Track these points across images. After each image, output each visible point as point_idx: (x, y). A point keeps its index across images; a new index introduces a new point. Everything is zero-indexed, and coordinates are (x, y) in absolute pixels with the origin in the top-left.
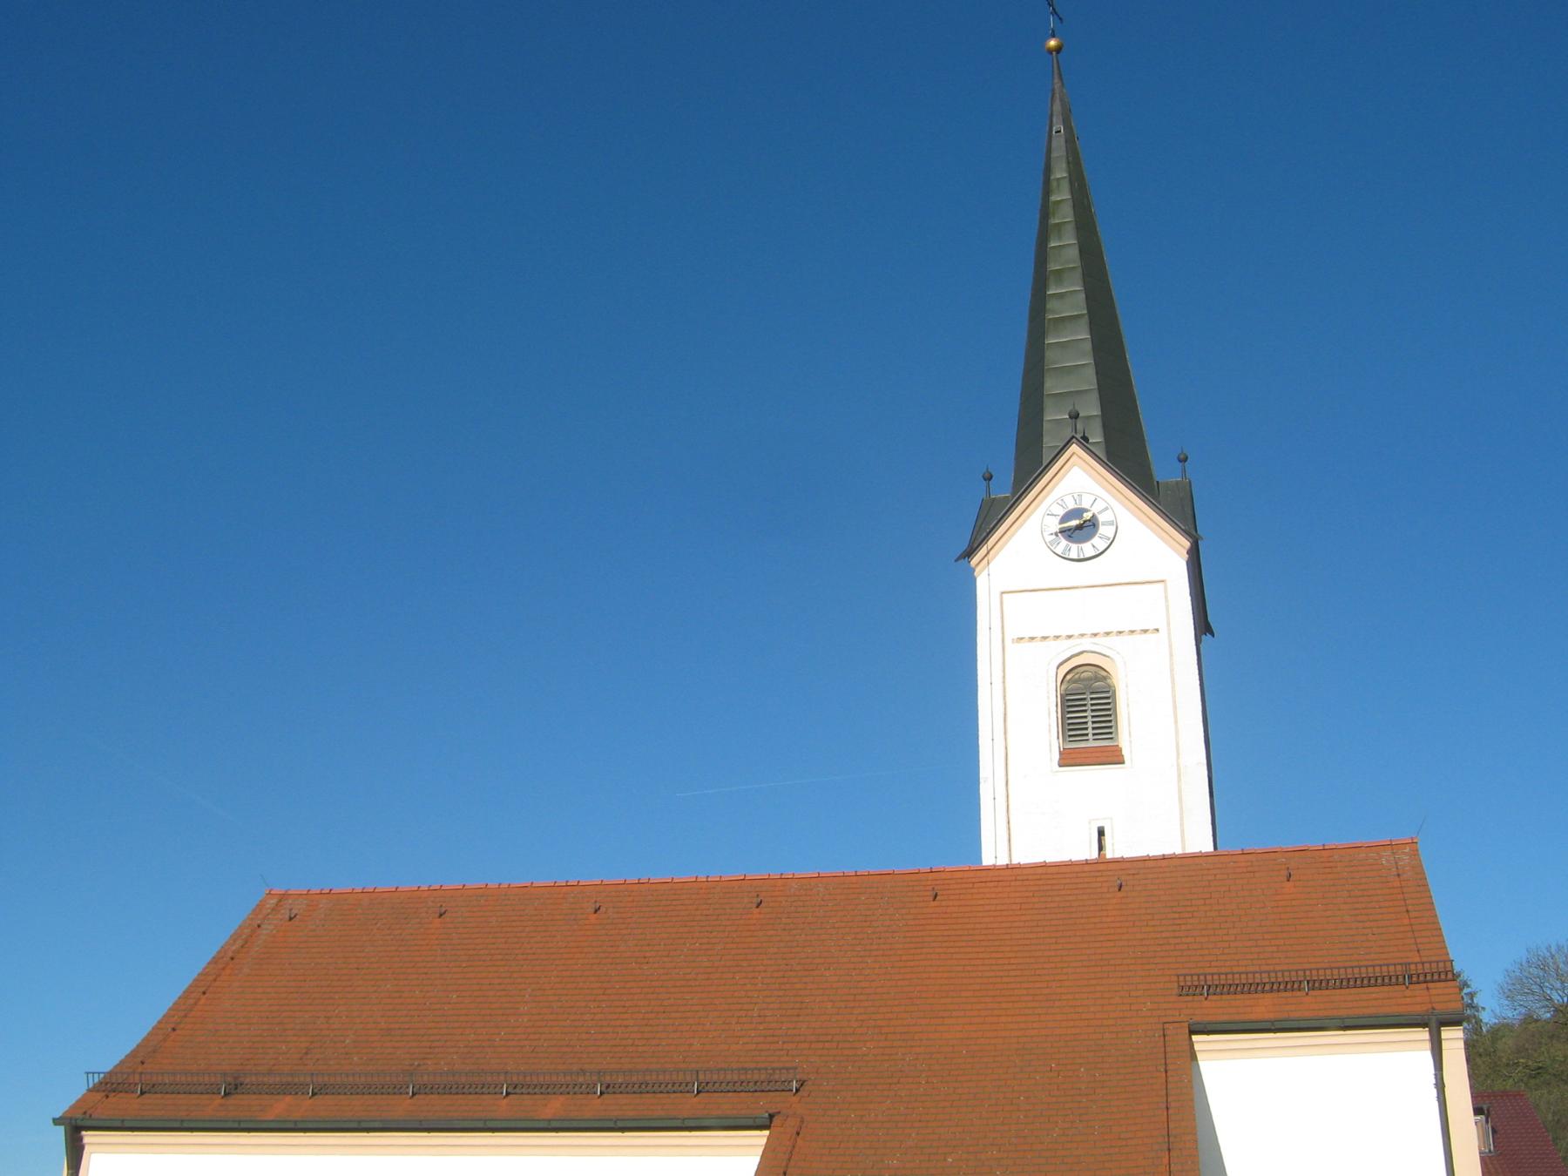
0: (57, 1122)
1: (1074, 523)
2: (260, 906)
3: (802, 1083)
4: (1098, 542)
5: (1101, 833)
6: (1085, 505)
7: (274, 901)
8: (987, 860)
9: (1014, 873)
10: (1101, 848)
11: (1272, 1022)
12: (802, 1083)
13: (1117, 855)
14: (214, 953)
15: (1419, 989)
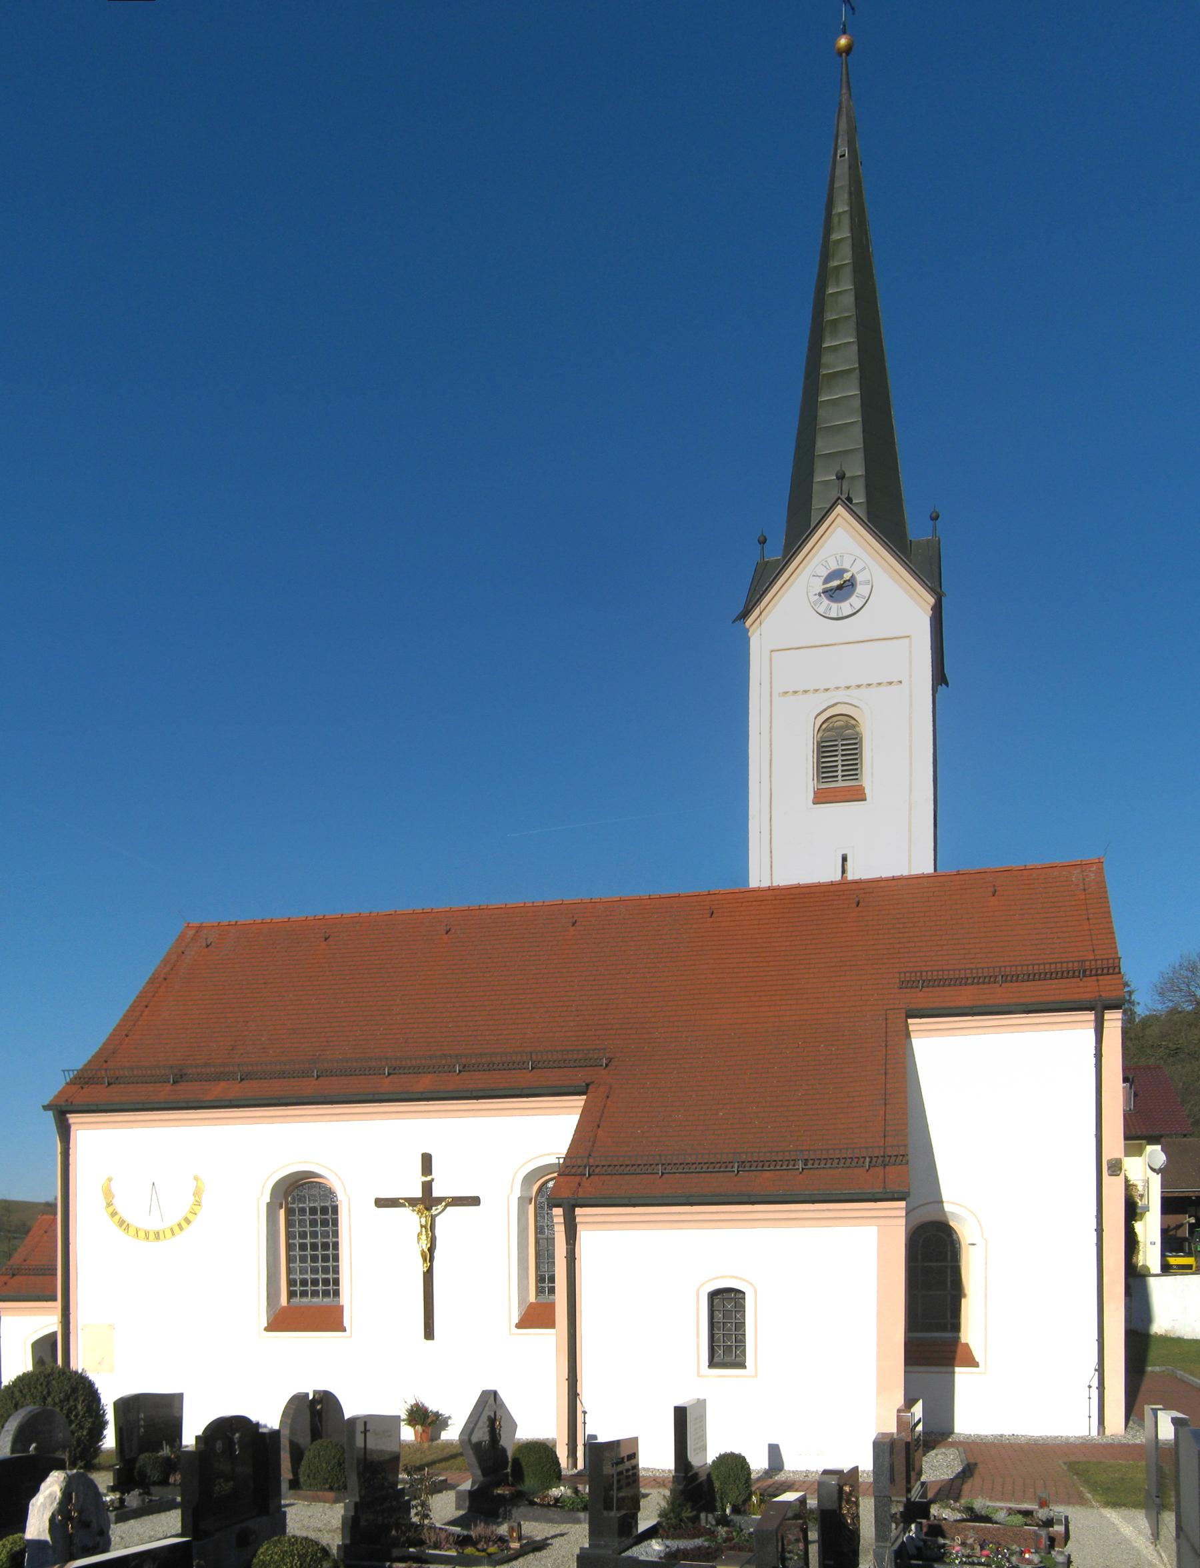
0: (46, 1108)
1: (836, 583)
2: (181, 937)
4: (855, 601)
5: (844, 859)
6: (846, 566)
7: (191, 933)
8: (754, 883)
10: (844, 871)
11: (972, 1008)
14: (150, 975)
15: (1090, 982)
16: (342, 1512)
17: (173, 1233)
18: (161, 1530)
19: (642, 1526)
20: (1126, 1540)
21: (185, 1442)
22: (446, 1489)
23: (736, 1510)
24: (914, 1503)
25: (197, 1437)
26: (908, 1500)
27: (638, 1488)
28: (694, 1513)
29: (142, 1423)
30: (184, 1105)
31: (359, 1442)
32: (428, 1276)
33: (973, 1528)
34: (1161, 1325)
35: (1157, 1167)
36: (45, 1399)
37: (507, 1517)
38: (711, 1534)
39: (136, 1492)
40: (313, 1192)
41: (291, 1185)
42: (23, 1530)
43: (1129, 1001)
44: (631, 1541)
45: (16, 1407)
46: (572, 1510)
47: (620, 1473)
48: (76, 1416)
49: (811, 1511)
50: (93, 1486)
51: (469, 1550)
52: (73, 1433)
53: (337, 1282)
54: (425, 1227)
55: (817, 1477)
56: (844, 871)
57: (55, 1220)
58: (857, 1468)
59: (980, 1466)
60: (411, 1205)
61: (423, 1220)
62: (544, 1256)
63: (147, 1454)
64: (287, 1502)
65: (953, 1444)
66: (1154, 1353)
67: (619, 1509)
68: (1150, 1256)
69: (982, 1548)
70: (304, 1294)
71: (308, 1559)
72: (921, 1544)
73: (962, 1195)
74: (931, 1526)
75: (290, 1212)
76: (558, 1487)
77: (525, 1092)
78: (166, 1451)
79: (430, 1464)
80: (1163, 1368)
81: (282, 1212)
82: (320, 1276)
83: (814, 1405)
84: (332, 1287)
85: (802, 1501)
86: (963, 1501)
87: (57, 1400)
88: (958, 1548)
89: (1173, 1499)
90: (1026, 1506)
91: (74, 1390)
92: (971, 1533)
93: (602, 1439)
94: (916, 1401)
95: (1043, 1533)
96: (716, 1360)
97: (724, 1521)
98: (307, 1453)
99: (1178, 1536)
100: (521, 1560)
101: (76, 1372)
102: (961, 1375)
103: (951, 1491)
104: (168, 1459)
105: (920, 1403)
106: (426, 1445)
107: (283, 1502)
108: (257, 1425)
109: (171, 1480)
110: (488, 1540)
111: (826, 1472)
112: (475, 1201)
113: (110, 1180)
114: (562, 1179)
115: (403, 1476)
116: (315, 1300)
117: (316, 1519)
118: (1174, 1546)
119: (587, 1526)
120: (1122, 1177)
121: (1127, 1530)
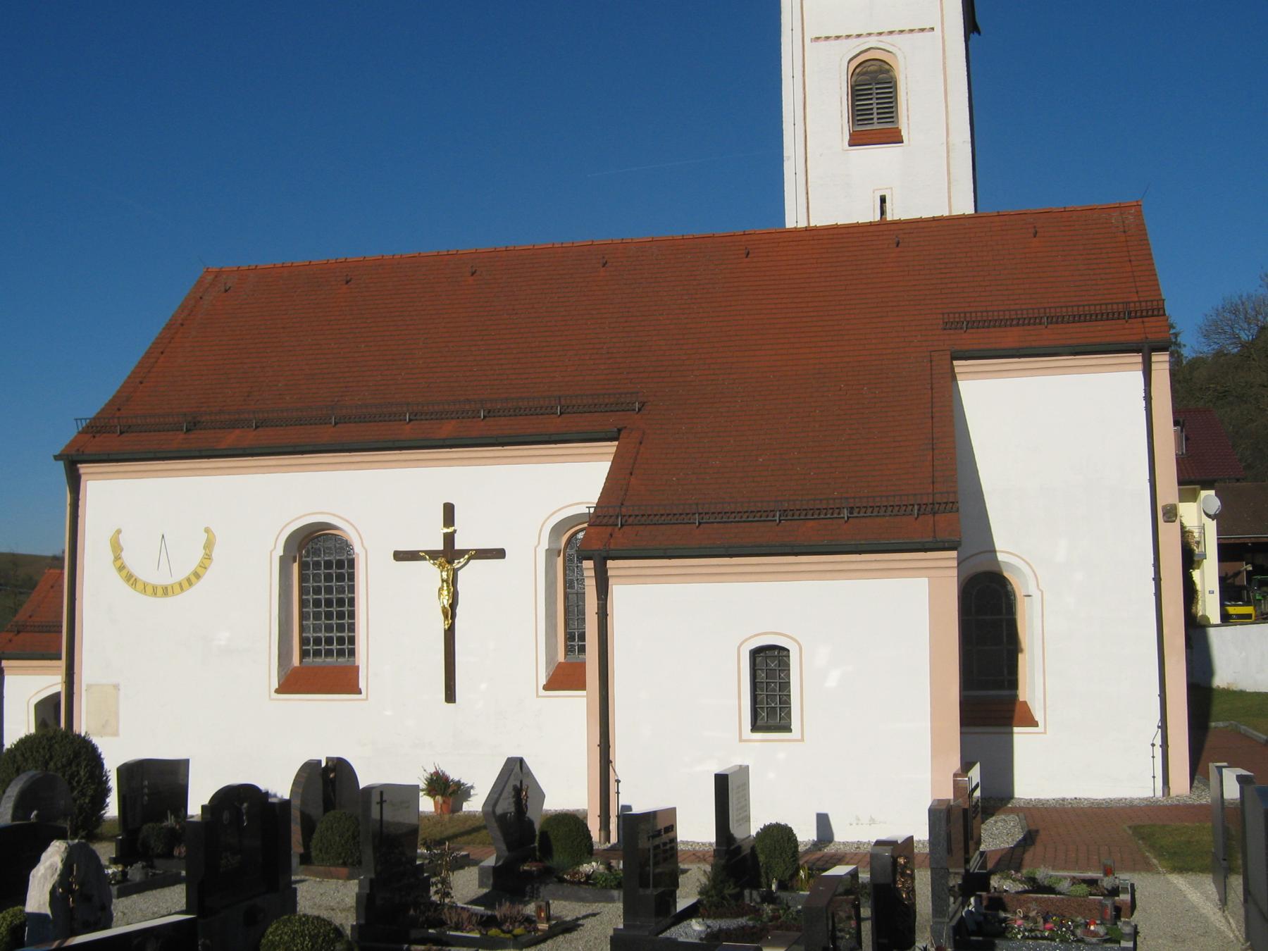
0: (57, 458)
2: (201, 282)
3: (643, 404)
5: (883, 200)
7: (210, 278)
8: (790, 224)
9: (812, 235)
10: (883, 212)
12: (643, 404)
13: (896, 218)
16: (356, 889)
17: (182, 589)
18: (163, 907)
19: (682, 904)
20: (1194, 907)
21: (190, 812)
22: (469, 865)
23: (783, 886)
24: (973, 874)
25: (203, 807)
26: (967, 871)
27: (676, 863)
28: (738, 890)
29: (146, 790)
30: (291, 449)
31: (375, 814)
32: (450, 635)
33: (1036, 900)
34: (1222, 679)
35: (1212, 513)
36: (47, 763)
37: (534, 896)
38: (756, 912)
39: (139, 865)
40: (330, 544)
41: (306, 537)
42: (23, 902)
43: (1175, 343)
44: (669, 921)
45: (18, 771)
46: (605, 887)
47: (657, 847)
48: (78, 782)
49: (864, 886)
50: (96, 858)
51: (493, 932)
52: (75, 800)
53: (352, 641)
54: (447, 581)
55: (869, 849)
56: (883, 212)
57: (62, 574)
58: (912, 837)
59: (1041, 832)
60: (431, 558)
61: (445, 574)
62: (574, 612)
63: (150, 825)
64: (298, 878)
65: (1013, 810)
66: (1217, 708)
67: (655, 886)
68: (1210, 606)
69: (1045, 921)
70: (317, 653)
71: (320, 941)
72: (982, 918)
73: (1014, 543)
74: (990, 899)
75: (303, 566)
76: (589, 863)
77: (553, 438)
78: (170, 821)
79: (450, 838)
80: (1227, 724)
81: (296, 566)
82: (335, 634)
83: (863, 769)
84: (347, 646)
85: (854, 875)
86: (1024, 871)
87: (59, 765)
88: (1020, 922)
89: (1240, 862)
90: (1090, 875)
91: (77, 755)
92: (1033, 905)
93: (637, 809)
94: (974, 764)
95: (1108, 902)
96: (759, 723)
97: (769, 898)
98: (319, 826)
99: (1246, 900)
100: (549, 942)
101: (79, 736)
102: (1021, 736)
103: (1011, 860)
104: (172, 830)
105: (978, 765)
106: (447, 817)
107: (293, 878)
108: (267, 794)
109: (176, 853)
110: (514, 920)
111: (878, 843)
112: (499, 554)
113: (119, 532)
114: (592, 530)
115: (422, 851)
116: (329, 660)
117: (329, 897)
118: (1242, 911)
119: (621, 905)
120: (1177, 523)
121: (1194, 896)
